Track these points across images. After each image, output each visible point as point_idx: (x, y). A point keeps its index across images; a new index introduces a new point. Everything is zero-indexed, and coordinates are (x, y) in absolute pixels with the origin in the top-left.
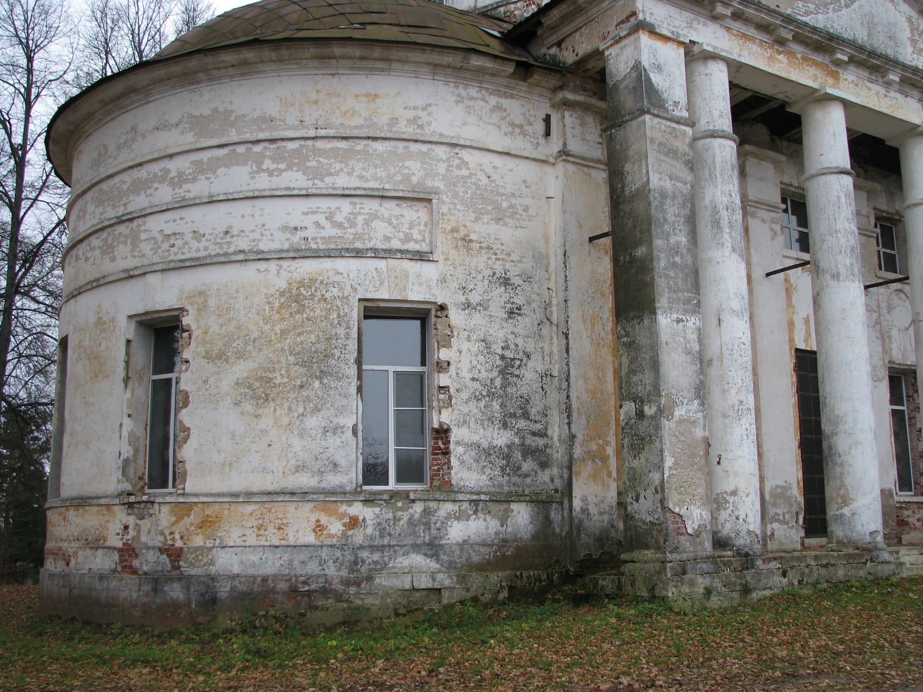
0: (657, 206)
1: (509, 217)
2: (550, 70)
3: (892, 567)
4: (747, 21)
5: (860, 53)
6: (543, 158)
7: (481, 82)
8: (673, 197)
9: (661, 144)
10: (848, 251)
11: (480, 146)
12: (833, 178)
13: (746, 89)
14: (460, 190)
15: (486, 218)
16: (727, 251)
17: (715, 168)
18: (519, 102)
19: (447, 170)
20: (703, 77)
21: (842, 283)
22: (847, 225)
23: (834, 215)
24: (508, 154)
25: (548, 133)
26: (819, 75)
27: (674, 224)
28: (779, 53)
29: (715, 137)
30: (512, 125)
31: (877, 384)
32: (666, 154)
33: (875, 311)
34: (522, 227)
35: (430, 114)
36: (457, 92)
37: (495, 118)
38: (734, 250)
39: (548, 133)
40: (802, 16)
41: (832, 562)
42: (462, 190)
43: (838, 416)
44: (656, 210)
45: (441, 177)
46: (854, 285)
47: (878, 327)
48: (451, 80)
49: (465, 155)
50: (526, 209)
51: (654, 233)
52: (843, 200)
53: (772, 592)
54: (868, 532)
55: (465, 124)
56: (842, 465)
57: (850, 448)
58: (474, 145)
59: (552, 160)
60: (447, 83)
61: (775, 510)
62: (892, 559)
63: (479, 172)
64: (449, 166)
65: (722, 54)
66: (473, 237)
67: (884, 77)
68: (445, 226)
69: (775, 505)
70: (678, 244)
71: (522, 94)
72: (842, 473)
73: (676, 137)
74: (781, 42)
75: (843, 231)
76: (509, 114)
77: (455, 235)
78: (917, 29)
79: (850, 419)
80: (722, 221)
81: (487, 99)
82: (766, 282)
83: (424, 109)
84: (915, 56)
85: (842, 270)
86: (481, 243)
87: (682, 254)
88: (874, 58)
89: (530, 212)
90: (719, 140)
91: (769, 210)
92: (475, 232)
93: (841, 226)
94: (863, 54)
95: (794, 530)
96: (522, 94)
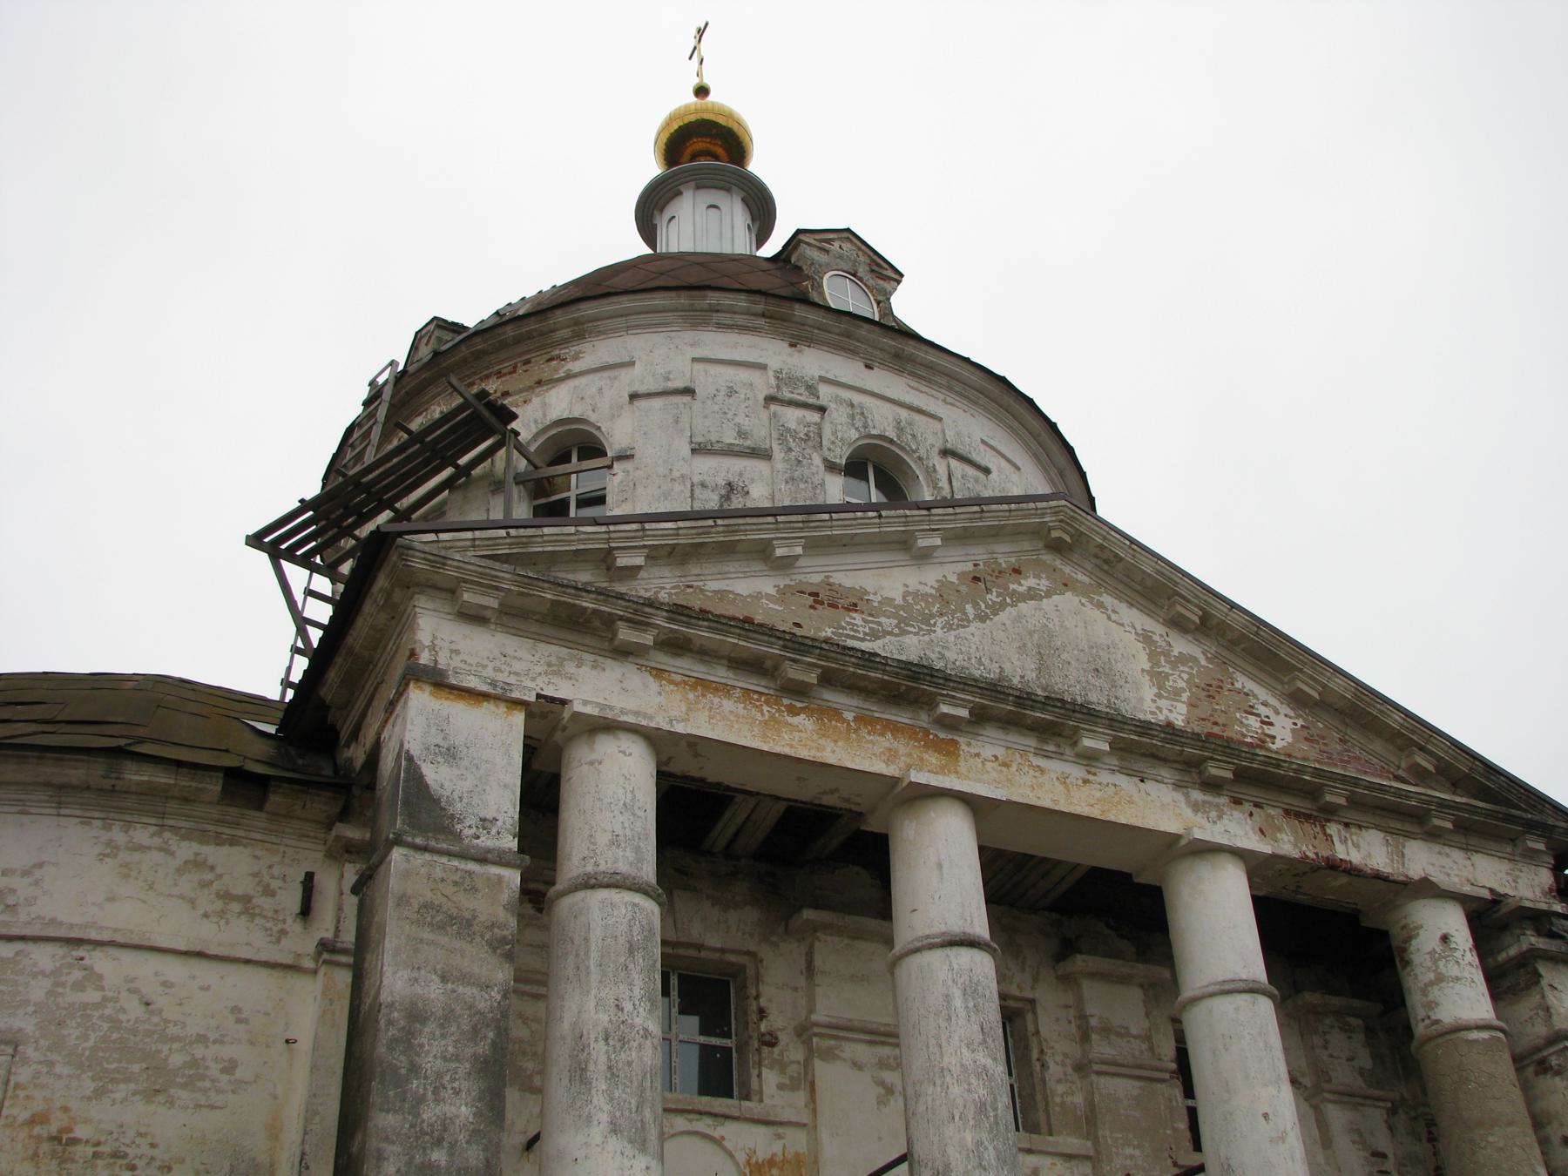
0: (395, 1040)
1: (183, 1086)
2: (307, 784)
4: (705, 654)
5: (996, 700)
6: (288, 960)
7: (163, 815)
8: (446, 1018)
9: (426, 906)
11: (136, 940)
12: (935, 958)
13: (778, 798)
14: (72, 1032)
15: (123, 1090)
16: (597, 1133)
17: (587, 953)
18: (248, 851)
19: (50, 993)
20: (585, 768)
22: (967, 1056)
23: (937, 1037)
24: (200, 955)
25: (306, 911)
26: (902, 750)
27: (439, 1075)
28: (793, 711)
29: (593, 887)
30: (226, 896)
32: (441, 928)
34: (212, 1107)
35: (36, 883)
36: (105, 836)
37: (187, 885)
38: (615, 1129)
39: (306, 911)
40: (862, 640)
42: (77, 1033)
44: (390, 1048)
45: (31, 1009)
48: (96, 814)
49: (100, 961)
50: (230, 1067)
51: (375, 1099)
52: (958, 1002)
55: (111, 899)
58: (119, 938)
59: (308, 964)
60: (86, 821)
63: (124, 994)
64: (56, 984)
65: (623, 718)
66: (81, 1132)
67: (1075, 744)
68: (15, 1111)
70: (445, 1123)
71: (258, 836)
73: (474, 889)
74: (797, 690)
75: (956, 1070)
76: (221, 876)
77: (37, 1130)
78: (1166, 654)
80: (591, 1067)
81: (173, 848)
83: (26, 873)
84: (1163, 703)
86: (98, 1144)
87: (452, 1145)
88: (1033, 708)
89: (239, 1073)
90: (603, 894)
91: (872, 1043)
92: (87, 1121)
94: (1005, 701)
96: (258, 836)
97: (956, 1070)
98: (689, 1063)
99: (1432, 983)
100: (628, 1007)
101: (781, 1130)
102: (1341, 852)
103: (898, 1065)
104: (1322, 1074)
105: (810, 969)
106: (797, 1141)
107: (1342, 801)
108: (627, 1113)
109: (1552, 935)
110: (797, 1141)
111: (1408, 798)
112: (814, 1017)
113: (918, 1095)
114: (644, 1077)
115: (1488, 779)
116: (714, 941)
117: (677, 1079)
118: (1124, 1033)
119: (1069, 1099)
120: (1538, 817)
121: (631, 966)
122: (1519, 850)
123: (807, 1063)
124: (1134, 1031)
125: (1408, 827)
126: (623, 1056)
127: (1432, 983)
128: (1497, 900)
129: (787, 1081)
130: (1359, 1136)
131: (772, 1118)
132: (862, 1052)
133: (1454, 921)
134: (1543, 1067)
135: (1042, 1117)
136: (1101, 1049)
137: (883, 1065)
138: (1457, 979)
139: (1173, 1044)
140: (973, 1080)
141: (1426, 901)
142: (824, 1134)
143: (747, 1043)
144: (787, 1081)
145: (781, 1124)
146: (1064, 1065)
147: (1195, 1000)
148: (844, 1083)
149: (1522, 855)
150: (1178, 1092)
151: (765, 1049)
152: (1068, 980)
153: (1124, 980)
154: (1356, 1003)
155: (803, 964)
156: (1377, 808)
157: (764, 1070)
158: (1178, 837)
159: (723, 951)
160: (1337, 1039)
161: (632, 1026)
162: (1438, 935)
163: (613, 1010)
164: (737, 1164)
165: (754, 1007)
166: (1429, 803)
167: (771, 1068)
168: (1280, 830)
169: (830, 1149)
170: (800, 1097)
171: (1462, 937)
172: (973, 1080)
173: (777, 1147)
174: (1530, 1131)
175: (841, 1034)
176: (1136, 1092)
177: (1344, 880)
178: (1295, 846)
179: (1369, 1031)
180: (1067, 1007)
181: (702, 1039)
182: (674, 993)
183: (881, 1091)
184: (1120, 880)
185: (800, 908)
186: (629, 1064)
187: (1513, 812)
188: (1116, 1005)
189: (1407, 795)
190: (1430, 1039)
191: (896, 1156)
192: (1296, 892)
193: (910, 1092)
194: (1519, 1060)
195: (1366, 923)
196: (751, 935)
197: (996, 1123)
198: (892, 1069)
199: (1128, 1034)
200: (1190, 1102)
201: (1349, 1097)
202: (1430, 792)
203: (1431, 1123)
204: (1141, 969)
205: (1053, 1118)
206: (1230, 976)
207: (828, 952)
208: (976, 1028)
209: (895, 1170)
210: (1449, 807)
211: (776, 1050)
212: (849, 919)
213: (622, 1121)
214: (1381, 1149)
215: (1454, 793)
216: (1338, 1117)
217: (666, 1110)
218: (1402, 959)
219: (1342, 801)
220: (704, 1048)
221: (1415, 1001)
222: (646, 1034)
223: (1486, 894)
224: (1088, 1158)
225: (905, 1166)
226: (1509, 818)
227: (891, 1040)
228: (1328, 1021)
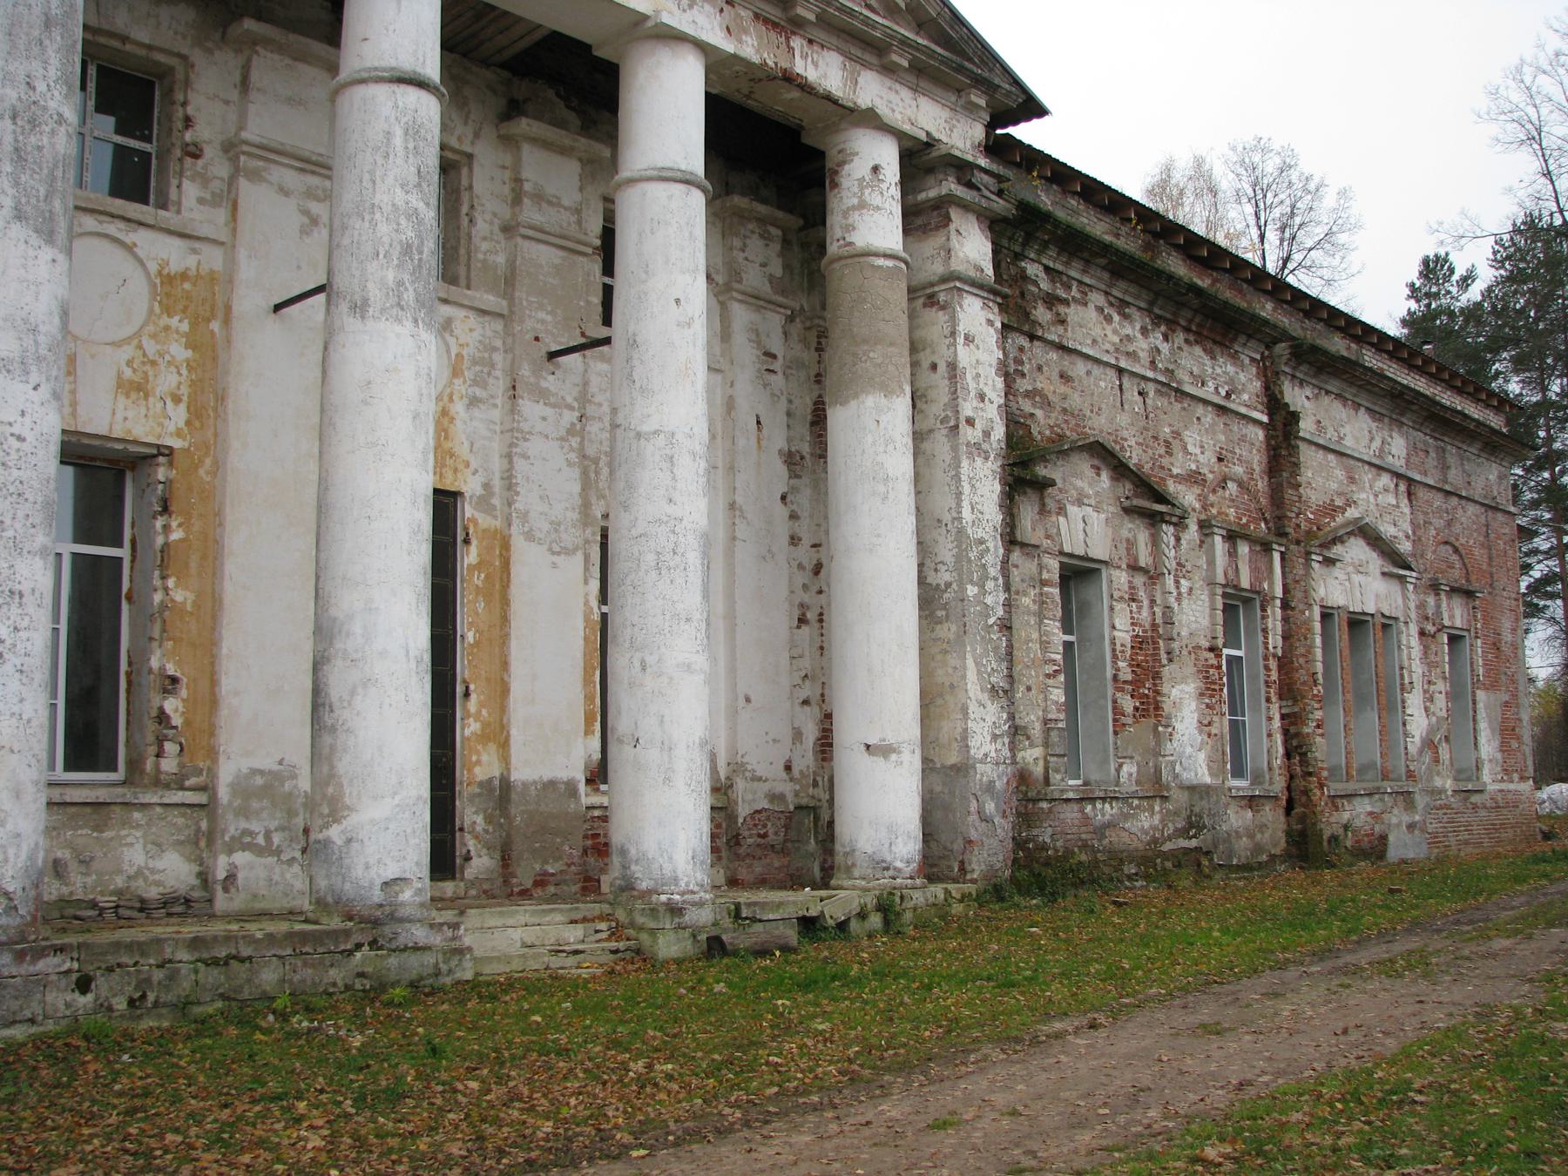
3: (429, 959)
10: (395, 254)
12: (381, 92)
21: (370, 324)
23: (372, 172)
31: (559, 560)
33: (571, 408)
38: (19, 215)
41: (246, 951)
43: (335, 619)
46: (398, 328)
47: (575, 441)
52: (398, 141)
53: (34, 1030)
54: (378, 882)
56: (333, 729)
57: (353, 693)
61: (243, 824)
62: (437, 940)
69: (244, 812)
72: (333, 748)
75: (387, 209)
79: (357, 628)
82: (272, 324)
85: (375, 293)
91: (302, 170)
93: (386, 198)
95: (296, 868)
97: (387, 209)
98: (102, 164)
99: (854, 208)
100: (41, 87)
101: (197, 245)
102: (801, 67)
103: (327, 197)
104: (735, 274)
105: (245, 84)
106: (213, 259)
107: (812, 17)
108: (33, 201)
109: (970, 185)
110: (213, 259)
111: (874, 28)
112: (244, 135)
113: (344, 227)
114: (56, 166)
115: (952, 28)
116: (142, 35)
117: (88, 177)
118: (555, 203)
119: (491, 258)
120: (986, 74)
121: (47, 42)
122: (962, 101)
123: (232, 181)
124: (566, 202)
125: (867, 57)
126: (33, 139)
127: (854, 208)
128: (930, 144)
129: (208, 197)
130: (756, 336)
131: (188, 231)
132: (291, 178)
133: (887, 154)
134: (931, 301)
135: (462, 271)
136: (531, 213)
137: (310, 194)
138: (878, 208)
139: (600, 222)
140: (403, 221)
141: (868, 131)
142: (242, 254)
143: (169, 151)
144: (208, 197)
145: (198, 238)
146: (491, 223)
147: (632, 181)
148: (268, 206)
149: (964, 108)
150: (596, 267)
151: (189, 160)
152: (509, 142)
153: (564, 151)
154: (780, 214)
155: (237, 77)
156: (843, 31)
157: (186, 184)
158: (645, 17)
159: (150, 47)
160: (755, 243)
161: (45, 108)
162: (871, 164)
163: (23, 87)
164: (148, 274)
165: (180, 113)
166: (891, 37)
167: (193, 179)
168: (746, 32)
169: (247, 270)
170: (221, 215)
171: (892, 172)
172: (403, 221)
173: (191, 262)
174: (906, 353)
175: (276, 158)
176: (557, 261)
177: (796, 94)
178: (758, 51)
179: (786, 242)
180: (504, 167)
181: (119, 139)
182: (92, 86)
183: (306, 220)
184: (581, 49)
185: (242, 16)
186: (40, 149)
187: (966, 64)
188: (553, 174)
189: (874, 25)
190: (841, 258)
191: (312, 286)
192: (748, 97)
193: (337, 223)
194: (912, 291)
195: (807, 140)
196: (184, 37)
197: (420, 266)
198: (319, 200)
199: (559, 205)
200: (607, 280)
201: (756, 300)
202: (896, 27)
203: (823, 334)
204: (583, 142)
205: (473, 274)
206: (669, 164)
207: (267, 69)
208: (413, 170)
209: (309, 301)
210: (910, 46)
211: (200, 162)
212: (292, 37)
213: (28, 209)
214: (773, 351)
215: (917, 34)
216: (741, 315)
217: (77, 208)
218: (832, 181)
219: (812, 17)
220: (120, 151)
221: (835, 221)
222: (61, 120)
223: (923, 137)
224: (501, 316)
225: (321, 297)
226: (960, 69)
227: (323, 171)
228: (750, 226)
